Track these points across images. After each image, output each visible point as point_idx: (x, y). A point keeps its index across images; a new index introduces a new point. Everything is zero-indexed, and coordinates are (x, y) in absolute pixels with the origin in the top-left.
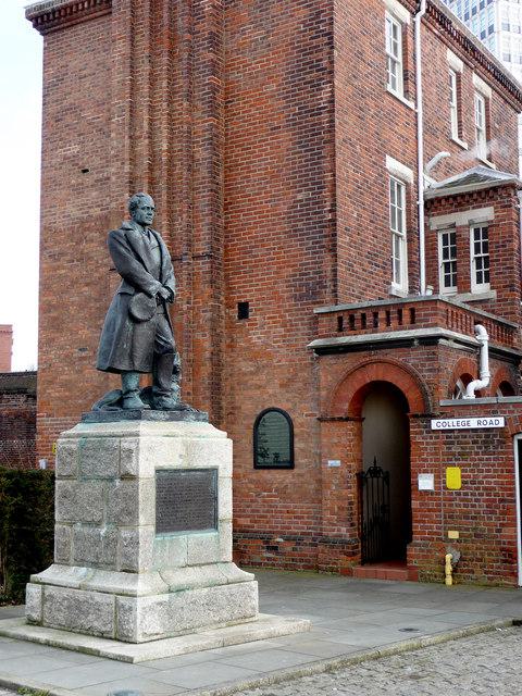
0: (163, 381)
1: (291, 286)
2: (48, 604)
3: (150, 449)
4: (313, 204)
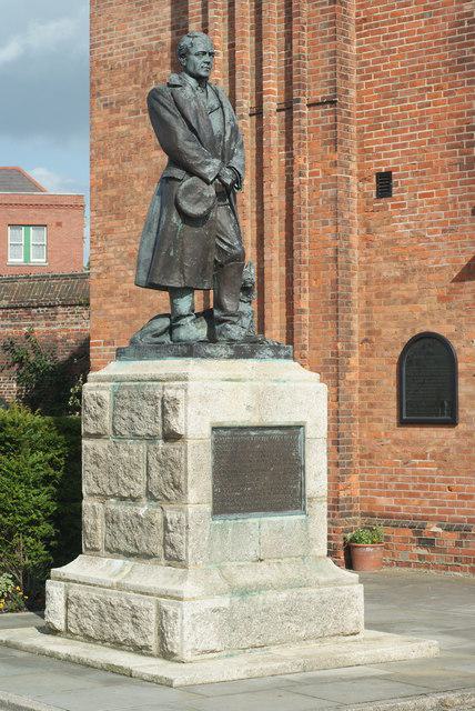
0: (228, 302)
1: (456, 146)
3: (204, 399)
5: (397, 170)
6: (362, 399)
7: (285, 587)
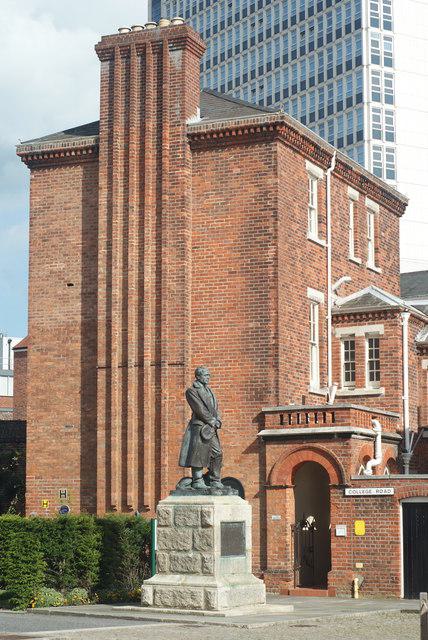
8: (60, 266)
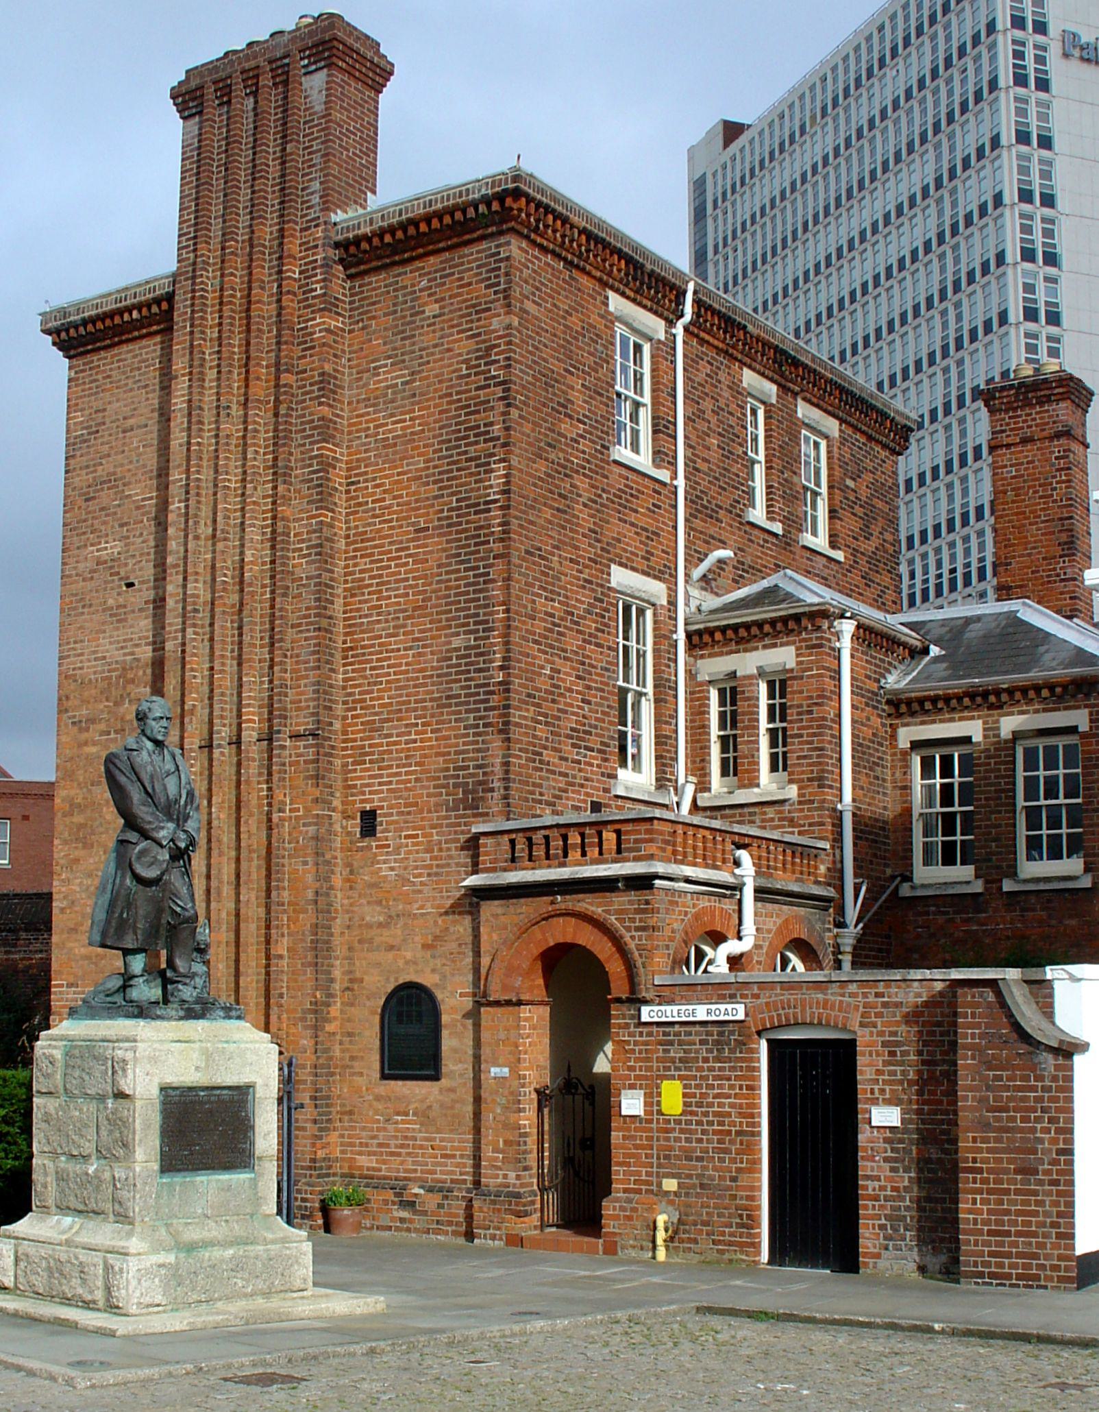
0: (180, 963)
1: (443, 786)
2: (22, 1265)
3: (153, 1060)
4: (477, 655)
5: (382, 808)
6: (343, 1051)
7: (231, 1244)
8: (112, 548)
